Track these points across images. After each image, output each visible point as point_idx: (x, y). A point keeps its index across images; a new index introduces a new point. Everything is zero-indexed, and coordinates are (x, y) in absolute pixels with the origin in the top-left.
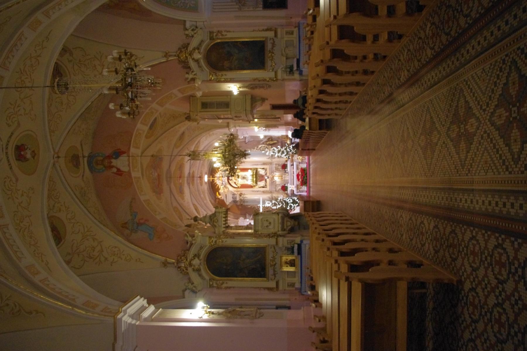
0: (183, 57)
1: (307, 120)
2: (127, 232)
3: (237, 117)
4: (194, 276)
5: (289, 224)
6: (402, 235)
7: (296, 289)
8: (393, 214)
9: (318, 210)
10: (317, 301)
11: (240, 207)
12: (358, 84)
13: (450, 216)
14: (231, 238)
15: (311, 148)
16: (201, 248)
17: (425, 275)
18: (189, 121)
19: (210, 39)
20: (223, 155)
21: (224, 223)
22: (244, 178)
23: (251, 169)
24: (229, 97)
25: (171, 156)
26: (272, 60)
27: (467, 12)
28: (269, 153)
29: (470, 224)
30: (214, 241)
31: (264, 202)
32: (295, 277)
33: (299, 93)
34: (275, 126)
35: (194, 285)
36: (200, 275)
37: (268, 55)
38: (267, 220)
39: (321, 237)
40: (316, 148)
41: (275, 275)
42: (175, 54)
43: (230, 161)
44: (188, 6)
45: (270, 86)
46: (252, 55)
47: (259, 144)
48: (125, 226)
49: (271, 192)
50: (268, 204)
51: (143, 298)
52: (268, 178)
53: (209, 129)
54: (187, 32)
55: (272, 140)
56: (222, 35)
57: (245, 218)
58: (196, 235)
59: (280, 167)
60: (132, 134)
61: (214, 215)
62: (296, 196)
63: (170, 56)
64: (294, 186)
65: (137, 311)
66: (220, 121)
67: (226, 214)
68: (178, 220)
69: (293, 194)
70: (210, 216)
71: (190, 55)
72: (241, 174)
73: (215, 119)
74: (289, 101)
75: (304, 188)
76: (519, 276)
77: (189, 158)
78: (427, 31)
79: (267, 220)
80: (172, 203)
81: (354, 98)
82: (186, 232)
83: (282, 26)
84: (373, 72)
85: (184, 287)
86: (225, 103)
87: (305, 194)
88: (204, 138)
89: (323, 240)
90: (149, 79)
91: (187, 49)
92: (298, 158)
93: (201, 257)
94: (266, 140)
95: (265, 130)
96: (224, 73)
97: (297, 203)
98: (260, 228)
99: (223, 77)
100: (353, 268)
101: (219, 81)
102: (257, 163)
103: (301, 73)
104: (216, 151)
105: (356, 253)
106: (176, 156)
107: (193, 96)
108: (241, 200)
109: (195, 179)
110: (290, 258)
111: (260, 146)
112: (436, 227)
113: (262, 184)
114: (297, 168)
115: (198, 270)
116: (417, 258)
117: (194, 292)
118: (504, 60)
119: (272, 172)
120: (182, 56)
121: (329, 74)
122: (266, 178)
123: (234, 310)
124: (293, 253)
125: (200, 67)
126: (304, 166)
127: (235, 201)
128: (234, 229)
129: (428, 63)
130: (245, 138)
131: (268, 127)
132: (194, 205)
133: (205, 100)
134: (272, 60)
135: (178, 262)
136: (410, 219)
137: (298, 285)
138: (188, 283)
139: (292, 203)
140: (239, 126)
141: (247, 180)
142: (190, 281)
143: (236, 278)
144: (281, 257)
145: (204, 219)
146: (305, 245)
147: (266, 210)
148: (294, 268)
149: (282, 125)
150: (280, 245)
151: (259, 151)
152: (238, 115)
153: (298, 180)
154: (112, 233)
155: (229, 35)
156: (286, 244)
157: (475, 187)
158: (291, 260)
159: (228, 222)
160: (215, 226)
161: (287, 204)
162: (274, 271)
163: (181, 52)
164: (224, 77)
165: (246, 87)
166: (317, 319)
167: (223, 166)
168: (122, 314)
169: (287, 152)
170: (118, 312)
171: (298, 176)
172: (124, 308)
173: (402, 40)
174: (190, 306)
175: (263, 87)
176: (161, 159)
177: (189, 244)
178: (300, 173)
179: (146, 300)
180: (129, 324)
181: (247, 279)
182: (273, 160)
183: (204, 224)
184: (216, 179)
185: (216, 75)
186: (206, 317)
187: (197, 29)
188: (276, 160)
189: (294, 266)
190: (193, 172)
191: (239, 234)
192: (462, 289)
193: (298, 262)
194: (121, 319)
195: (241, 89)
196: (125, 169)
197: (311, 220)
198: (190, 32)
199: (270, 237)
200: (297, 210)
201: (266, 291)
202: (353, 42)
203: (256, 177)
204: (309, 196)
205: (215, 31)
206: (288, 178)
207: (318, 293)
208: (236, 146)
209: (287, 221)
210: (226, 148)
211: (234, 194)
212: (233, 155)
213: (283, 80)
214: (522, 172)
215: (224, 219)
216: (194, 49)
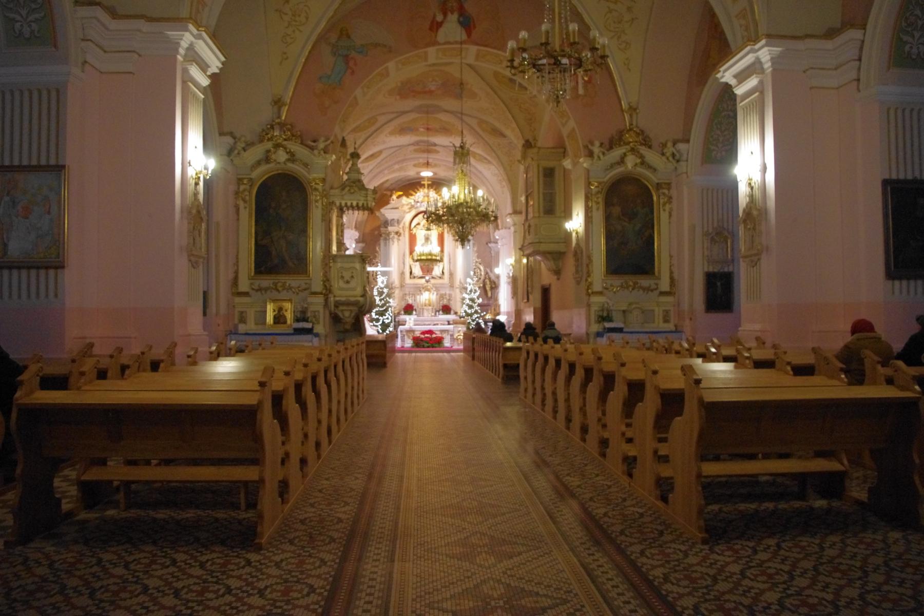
0: (627, 137)
1: (521, 345)
2: (333, 37)
3: (528, 228)
4: (257, 152)
5: (347, 315)
6: (327, 479)
7: (236, 327)
8: (360, 468)
9: (369, 365)
10: (216, 356)
11: (376, 233)
12: (569, 420)
13: (356, 537)
14: (323, 216)
15: (477, 354)
16: (306, 165)
17: (268, 499)
18: (524, 146)
19: (658, 184)
20: (461, 204)
21: (349, 204)
22: (427, 239)
23: (442, 251)
24: (563, 215)
25: (462, 114)
26: (622, 286)
27: (703, 610)
28: (471, 284)
29: (344, 559)
30: (317, 186)
31: (384, 274)
32: (256, 324)
33: (568, 332)
34: (515, 293)
35: (242, 152)
36: (259, 163)
37: (630, 280)
38: (352, 277)
39: (325, 358)
40: (476, 362)
41: (260, 289)
42: (634, 123)
43: (453, 215)
44: (712, 148)
45: (578, 283)
46: (631, 254)
47: (485, 267)
48: (344, 34)
49: (402, 286)
50: (381, 281)
51: (220, 66)
52: (427, 281)
53: (512, 182)
54: (670, 144)
55: (492, 288)
56: (664, 204)
57: (357, 241)
58: (327, 156)
59: (445, 302)
60: (499, 50)
61: (362, 187)
62: (396, 328)
63: (631, 116)
64: (411, 325)
65: (199, 56)
66: (523, 199)
67: (364, 208)
68: (354, 126)
69: (398, 324)
70: (360, 181)
71: (632, 150)
72: (434, 233)
73: (527, 191)
74: (556, 317)
75: (409, 343)
76: (271, 610)
77: (458, 145)
78: (673, 545)
79: (352, 277)
80: (384, 114)
81: (549, 416)
82: (332, 138)
83: (679, 305)
84: (584, 440)
85: (238, 135)
86: (554, 208)
87: (399, 344)
88: (497, 172)
89: (319, 360)
90: (565, 91)
91: (642, 144)
92: (460, 331)
93: (290, 165)
94: (493, 278)
95: (509, 277)
96: (601, 206)
97: (384, 331)
98: (339, 265)
99: (594, 204)
100: (278, 399)
101: (587, 199)
102: (452, 261)
103: (599, 335)
104: (470, 193)
105: (300, 405)
106: (462, 120)
107: (564, 154)
108: (389, 234)
109: (425, 155)
110: (289, 316)
111: (482, 268)
112: (340, 520)
113: (417, 271)
114: (442, 331)
115: (267, 160)
116: (295, 494)
117: (230, 153)
118: (571, 592)
119: (437, 289)
120: (631, 137)
121: (583, 372)
122: (427, 278)
123: (202, 219)
124: (297, 320)
125: (612, 166)
126: (447, 343)
127: (386, 223)
128: (337, 221)
129: (637, 569)
130: (496, 242)
131: (514, 281)
132: (380, 152)
133: (558, 175)
134: (622, 286)
135: (282, 125)
136: (352, 490)
137: (242, 328)
138: (245, 142)
139: (383, 322)
140: (515, 232)
141: (423, 245)
142: (249, 145)
143: (253, 223)
144: (290, 300)
145: (355, 170)
146: (311, 341)
147: (371, 278)
148: (272, 322)
149: (517, 304)
150: (312, 299)
151: (473, 266)
152: (532, 230)
153: (424, 333)
154: (330, 13)
155: (664, 216)
156: (312, 308)
157: (397, 565)
158: (285, 317)
159: (350, 212)
160: (343, 189)
161: (382, 314)
162: (266, 289)
163: (638, 134)
164: (595, 207)
165: (577, 244)
166: (192, 353)
167: (444, 203)
168: (195, 31)
169: (471, 315)
170: (198, 26)
171: (430, 332)
172: (204, 34)
173: (625, 478)
174: (208, 145)
175: (577, 272)
176: (459, 97)
177: (313, 144)
178: (434, 336)
179: (217, 71)
180: (178, 44)
181: (253, 242)
182: (458, 291)
183: (347, 170)
184: (426, 190)
185: (598, 193)
186: (191, 172)
187: (674, 162)
188: (457, 295)
189: (275, 323)
190: (438, 152)
191: (329, 230)
192: (248, 551)
193: (280, 329)
194: (187, 30)
195: (574, 235)
196: (442, 35)
197: (353, 346)
198: (670, 150)
199: (324, 282)
200: (371, 330)
201: (231, 276)
202: (624, 404)
203: (427, 260)
204: (394, 350)
205: (671, 191)
206: (428, 315)
207: (233, 356)
208: (476, 225)
209: (351, 311)
210: (474, 208)
211: (398, 222)
212: (462, 220)
213: (589, 305)
214: (413, 612)
215: (355, 204)
216: (642, 157)
